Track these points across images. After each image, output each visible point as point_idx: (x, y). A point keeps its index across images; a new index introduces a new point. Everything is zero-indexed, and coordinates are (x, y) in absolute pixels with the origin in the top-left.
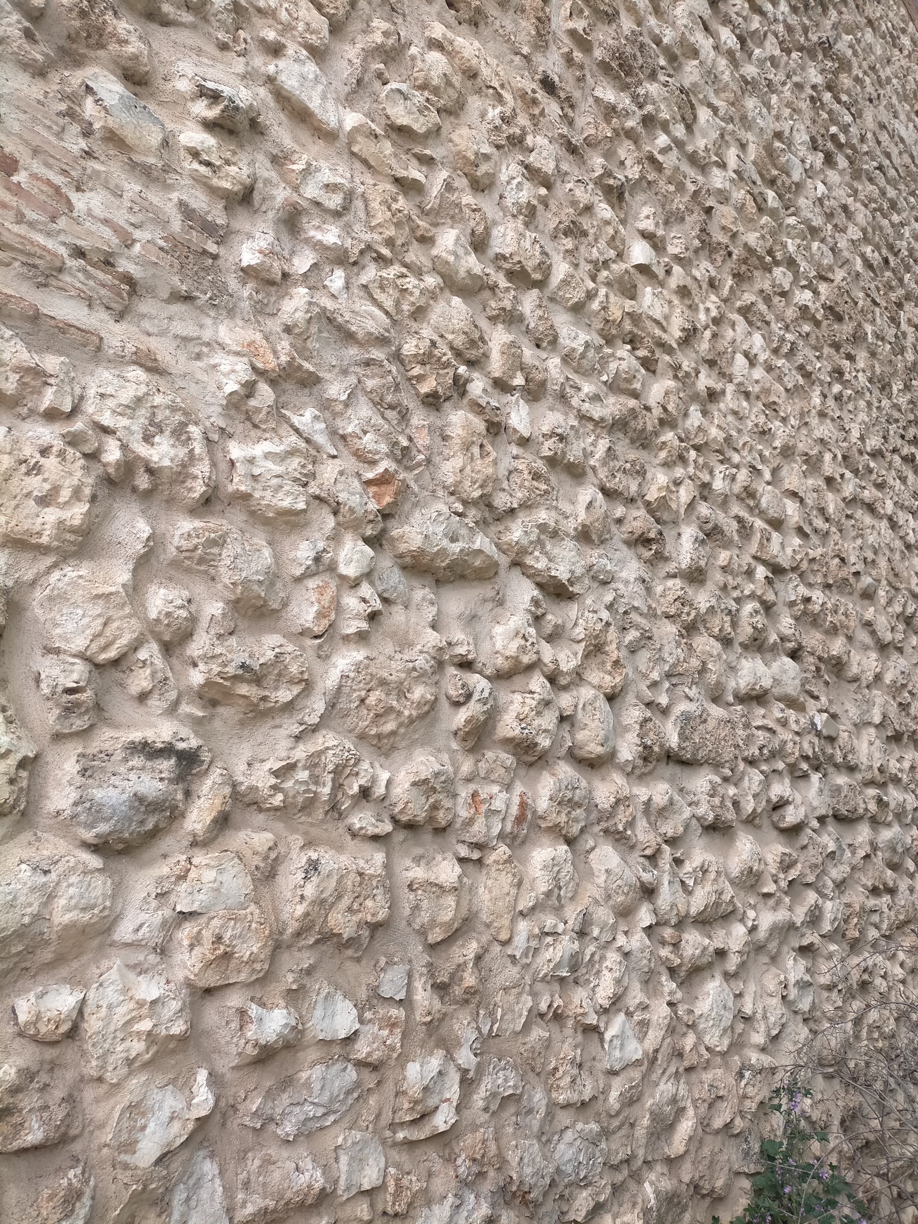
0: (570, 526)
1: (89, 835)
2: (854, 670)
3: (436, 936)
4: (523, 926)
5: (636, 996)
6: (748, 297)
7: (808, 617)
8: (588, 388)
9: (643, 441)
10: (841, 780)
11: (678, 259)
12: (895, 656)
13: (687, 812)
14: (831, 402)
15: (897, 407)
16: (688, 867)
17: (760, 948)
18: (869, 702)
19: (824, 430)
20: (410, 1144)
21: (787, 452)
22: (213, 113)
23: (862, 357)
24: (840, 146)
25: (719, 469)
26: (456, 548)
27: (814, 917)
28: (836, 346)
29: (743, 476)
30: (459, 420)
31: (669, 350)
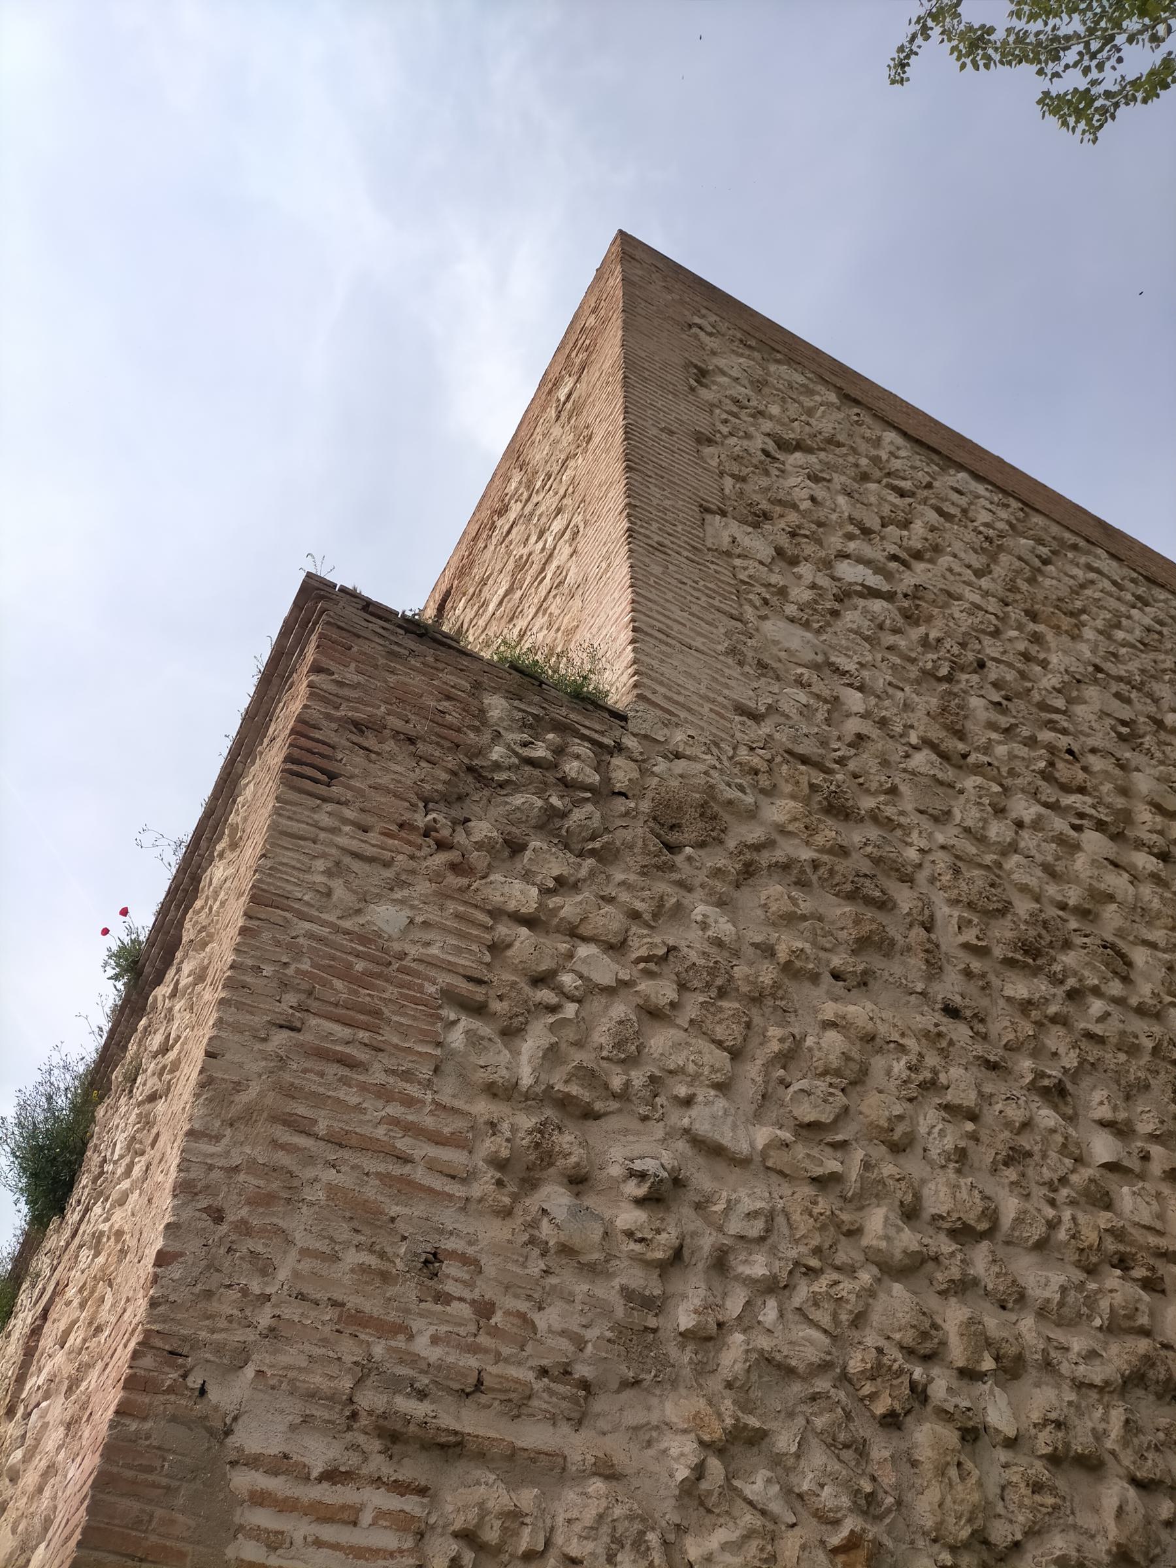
8: (1078, 1344)
22: (642, 1191)
30: (928, 1437)
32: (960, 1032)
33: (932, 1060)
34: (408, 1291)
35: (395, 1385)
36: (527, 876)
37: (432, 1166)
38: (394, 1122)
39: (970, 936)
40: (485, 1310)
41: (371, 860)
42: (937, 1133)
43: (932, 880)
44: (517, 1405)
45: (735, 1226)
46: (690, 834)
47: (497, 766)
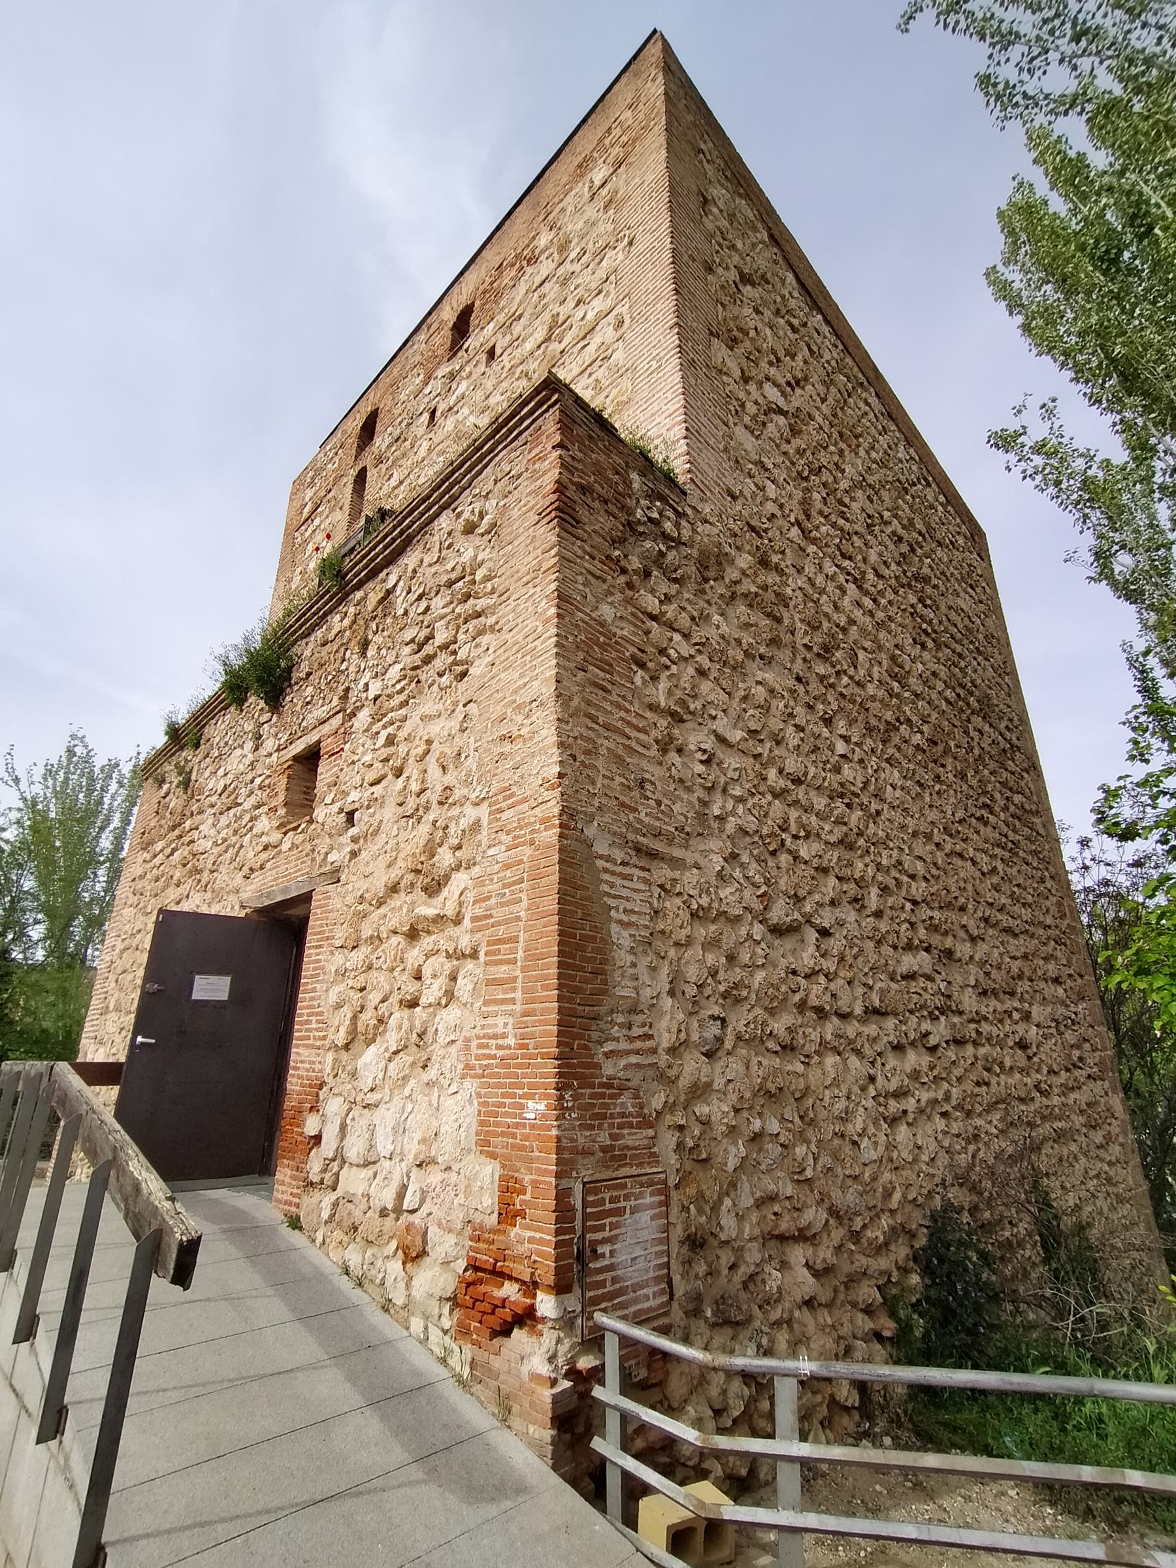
0: (827, 899)
1: (703, 1050)
2: (959, 955)
3: (798, 1095)
4: (827, 1092)
5: (871, 1130)
6: (891, 751)
7: (933, 928)
8: (827, 828)
9: (851, 847)
10: (956, 1019)
11: (856, 744)
12: (980, 943)
13: (885, 1039)
14: (935, 796)
15: (971, 787)
16: (888, 1067)
17: (922, 1111)
18: (968, 973)
19: (932, 815)
20: (798, 1181)
21: (915, 834)
22: (704, 757)
23: (949, 761)
24: (928, 635)
25: (885, 853)
26: (788, 919)
27: (947, 1097)
28: (935, 762)
29: (895, 853)
30: (784, 859)
31: (857, 795)
32: (801, 689)
33: (792, 703)
34: (636, 793)
35: (637, 831)
36: (653, 591)
37: (638, 741)
38: (622, 719)
39: (806, 641)
40: (659, 803)
41: (597, 578)
42: (792, 737)
43: (796, 607)
44: (671, 842)
45: (730, 774)
46: (712, 574)
47: (639, 522)
